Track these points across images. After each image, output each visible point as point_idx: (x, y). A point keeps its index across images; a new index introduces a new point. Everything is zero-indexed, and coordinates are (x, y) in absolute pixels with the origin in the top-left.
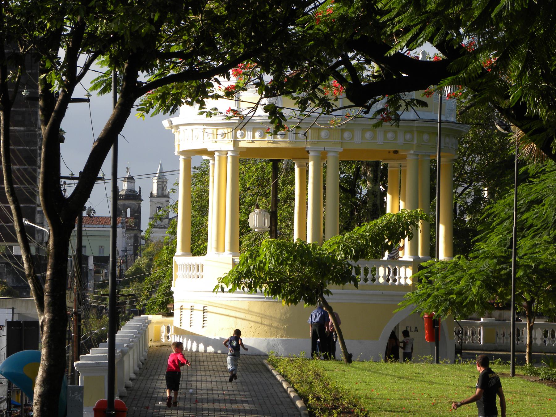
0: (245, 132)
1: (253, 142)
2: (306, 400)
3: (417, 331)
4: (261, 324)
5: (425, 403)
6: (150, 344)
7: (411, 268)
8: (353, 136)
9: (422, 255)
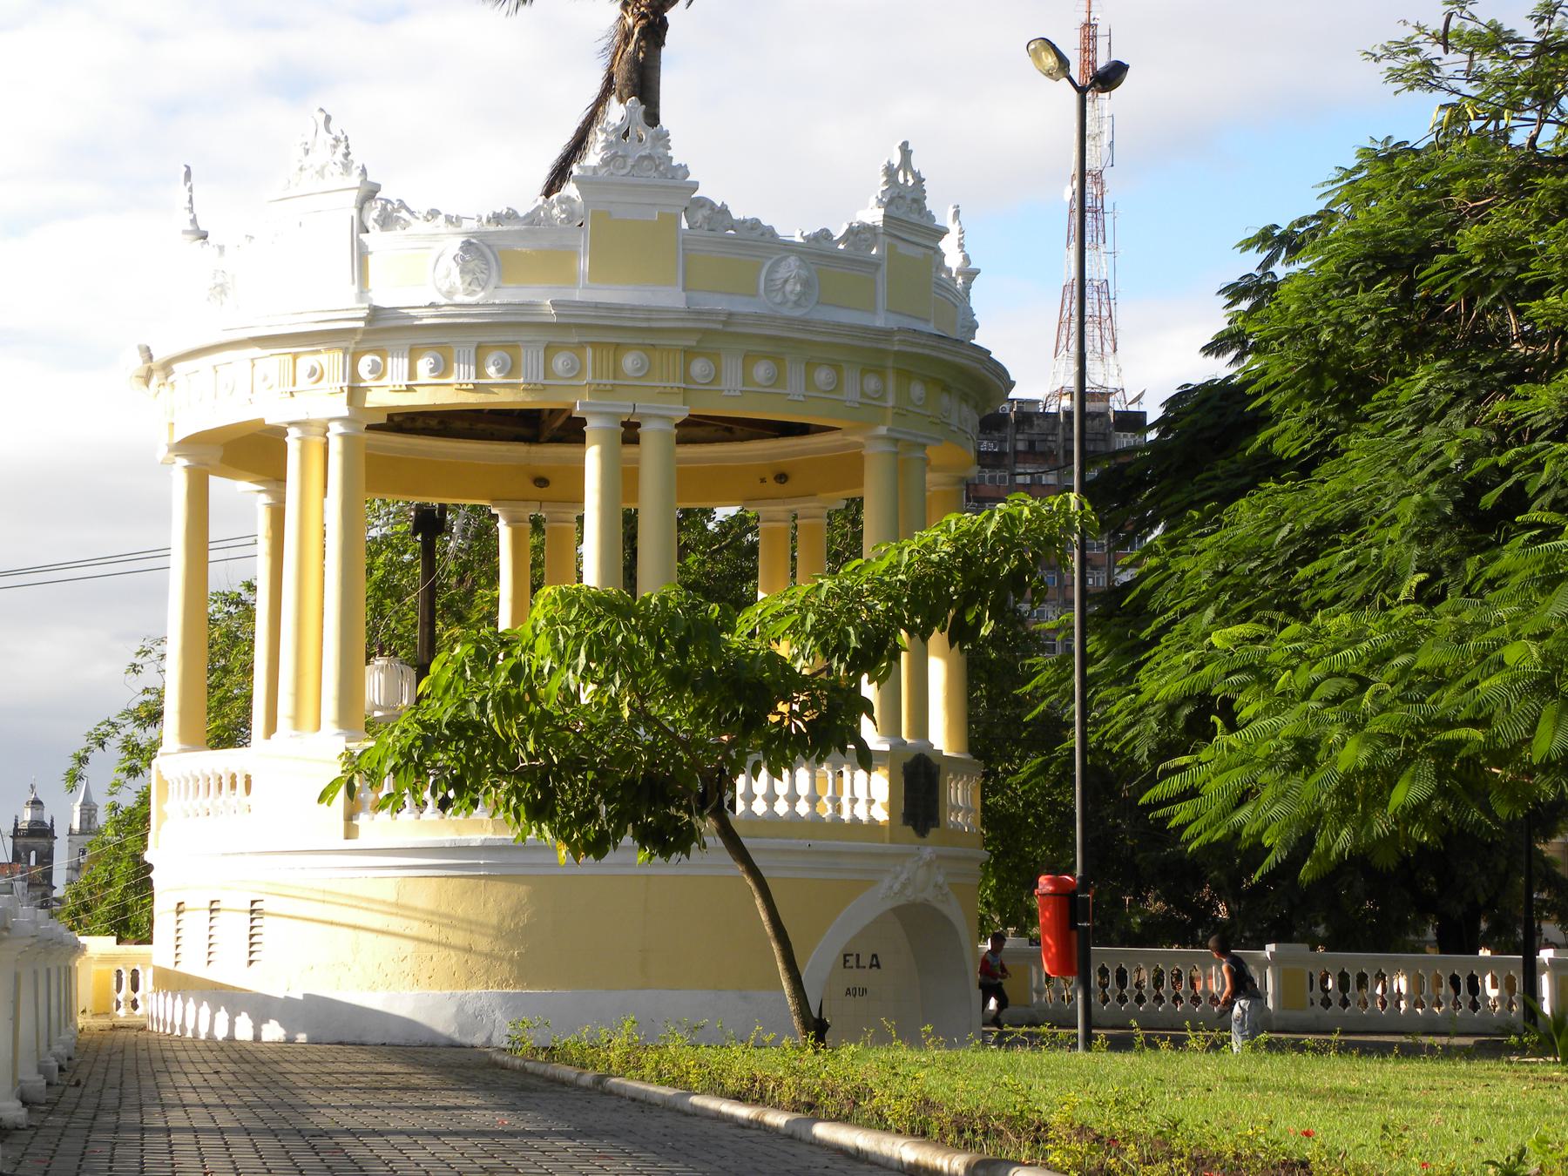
0: (384, 360)
1: (409, 388)
3: (878, 966)
4: (439, 944)
6: (81, 1021)
7: (886, 772)
9: (910, 736)
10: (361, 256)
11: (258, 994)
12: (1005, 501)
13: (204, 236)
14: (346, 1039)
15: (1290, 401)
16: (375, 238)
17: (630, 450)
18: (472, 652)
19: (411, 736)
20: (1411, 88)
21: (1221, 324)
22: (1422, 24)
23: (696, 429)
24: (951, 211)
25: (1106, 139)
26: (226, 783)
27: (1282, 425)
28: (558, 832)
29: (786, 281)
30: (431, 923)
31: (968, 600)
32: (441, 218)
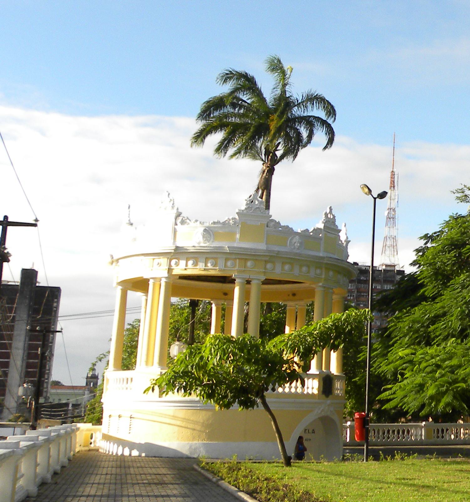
0: (179, 261)
1: (185, 269)
3: (314, 432)
7: (318, 380)
8: (274, 267)
9: (325, 369)
10: (175, 231)
11: (131, 442)
12: (348, 310)
13: (132, 224)
14: (156, 456)
15: (429, 281)
16: (179, 227)
17: (248, 286)
18: (189, 352)
19: (171, 375)
20: (461, 202)
21: (415, 258)
22: (466, 185)
23: (267, 282)
24: (344, 224)
25: (396, 200)
26: (122, 380)
27: (427, 288)
28: (215, 402)
29: (295, 243)
30: (183, 421)
31: (336, 338)
32: (198, 222)
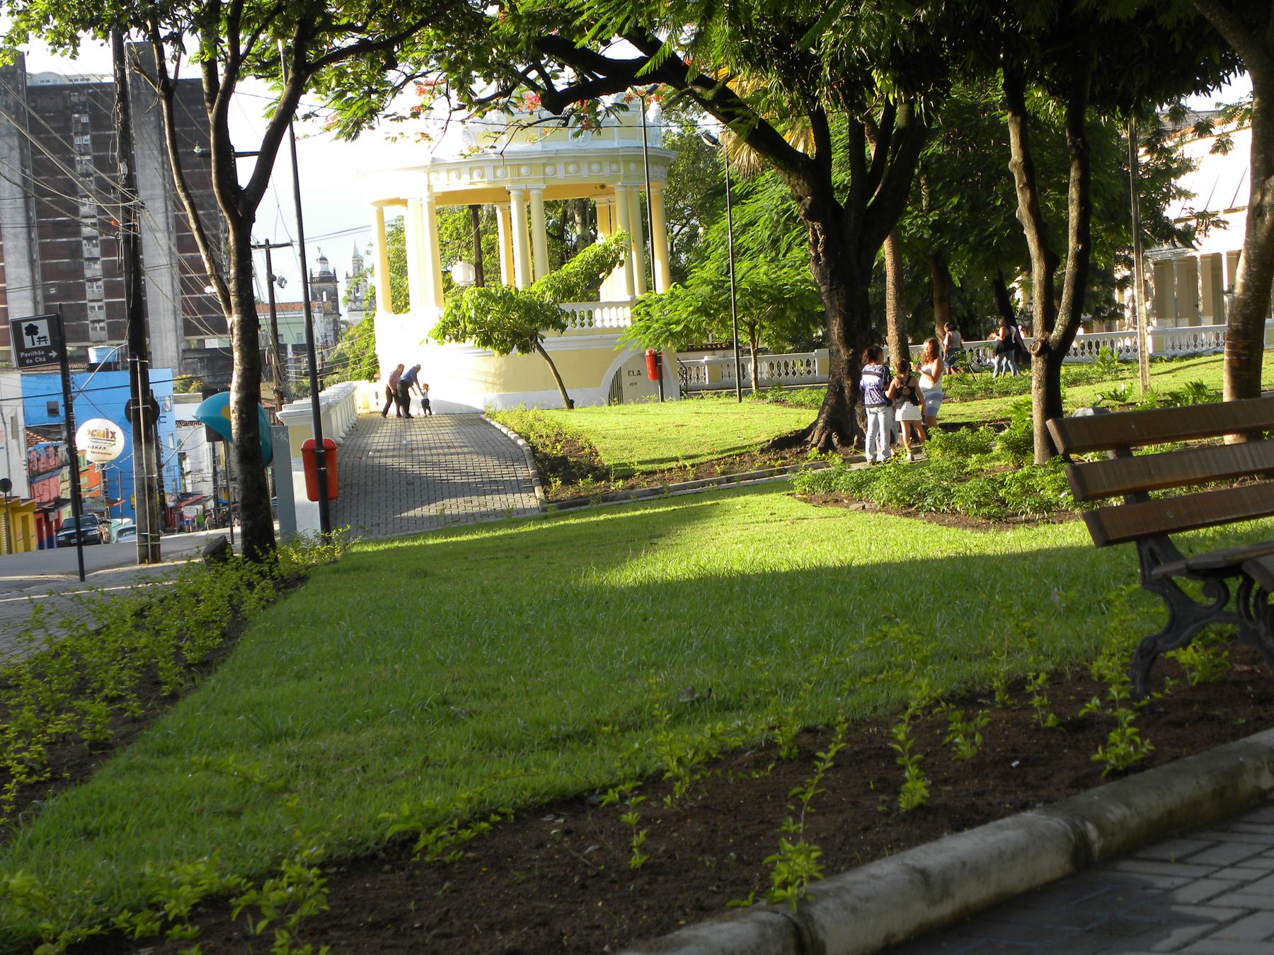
2: (527, 439)
5: (651, 429)
6: (359, 411)
